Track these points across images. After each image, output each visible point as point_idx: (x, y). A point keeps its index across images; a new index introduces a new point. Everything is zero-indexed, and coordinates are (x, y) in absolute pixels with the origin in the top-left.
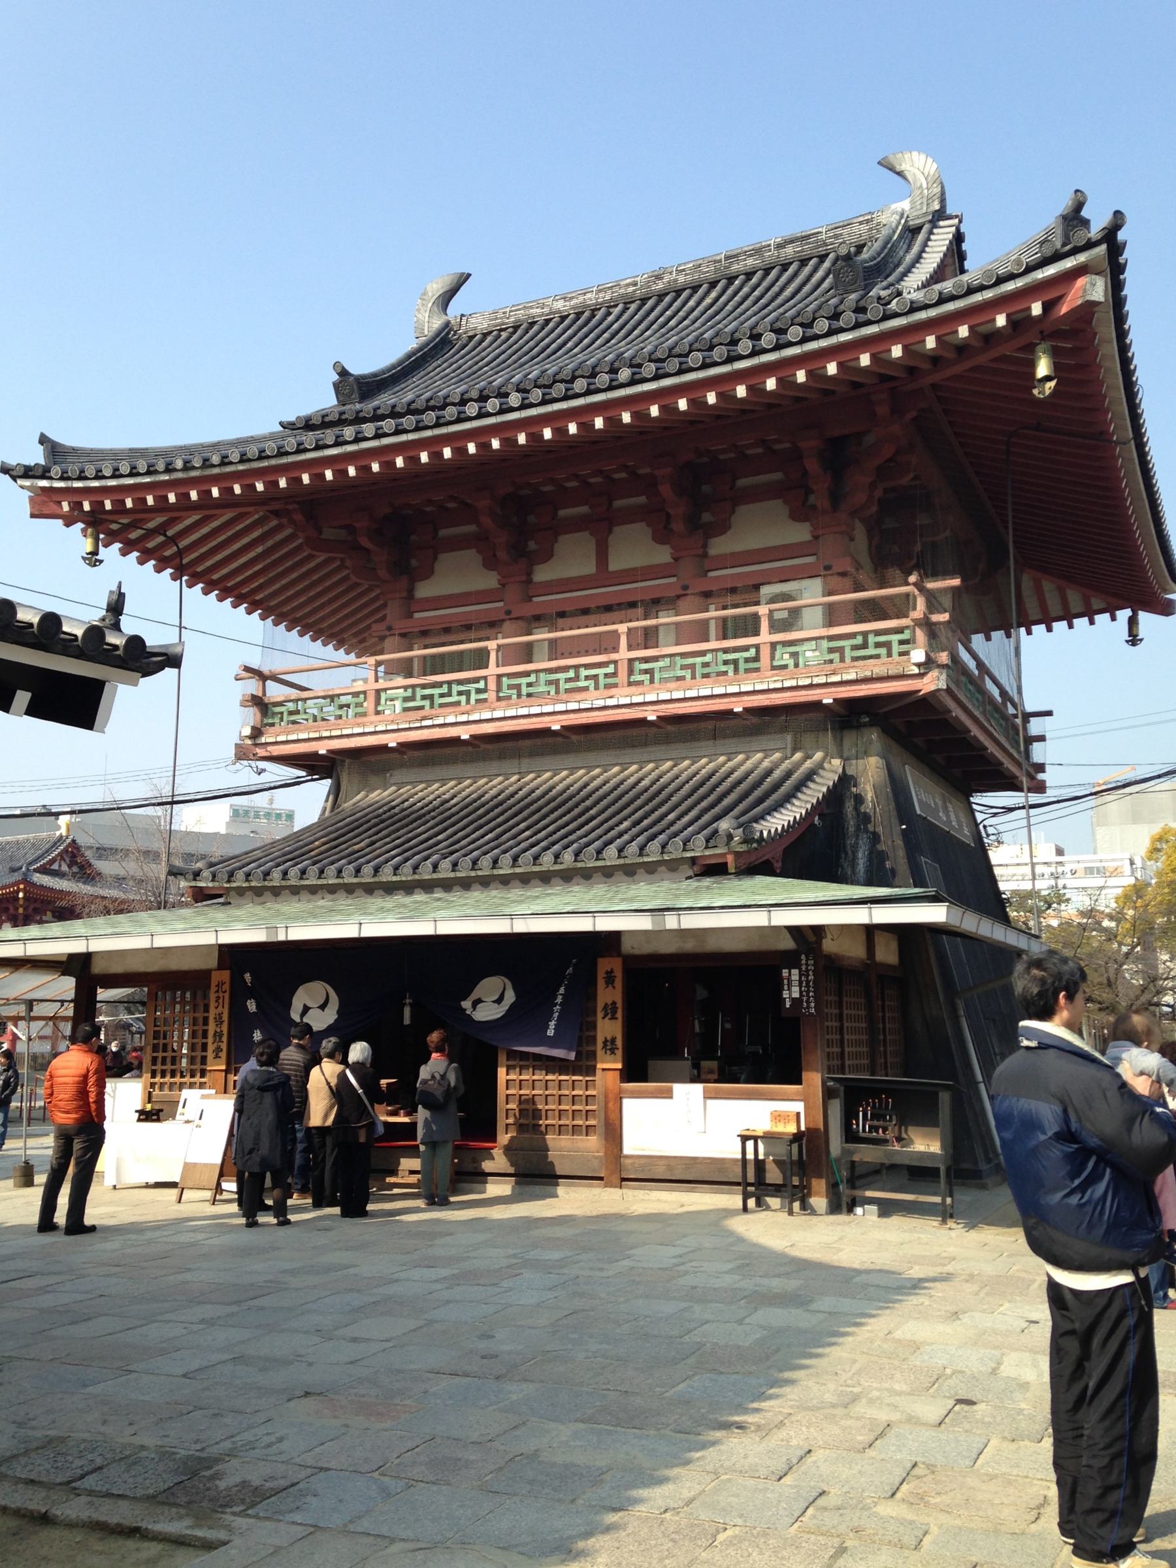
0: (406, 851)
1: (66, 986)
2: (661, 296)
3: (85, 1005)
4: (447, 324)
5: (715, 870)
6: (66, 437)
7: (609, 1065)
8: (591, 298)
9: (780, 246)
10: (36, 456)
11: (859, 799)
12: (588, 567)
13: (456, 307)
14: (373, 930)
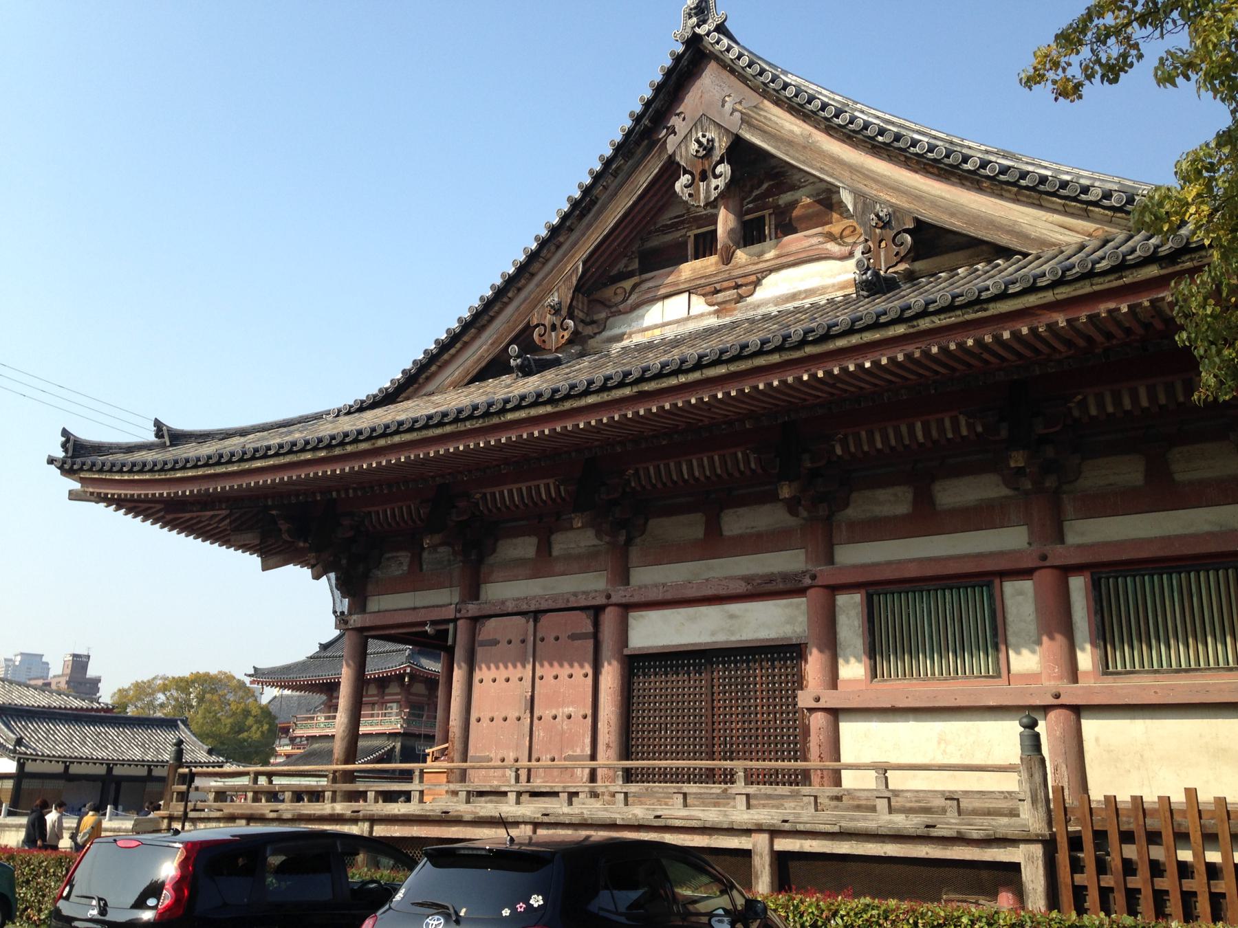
10: (252, 672)
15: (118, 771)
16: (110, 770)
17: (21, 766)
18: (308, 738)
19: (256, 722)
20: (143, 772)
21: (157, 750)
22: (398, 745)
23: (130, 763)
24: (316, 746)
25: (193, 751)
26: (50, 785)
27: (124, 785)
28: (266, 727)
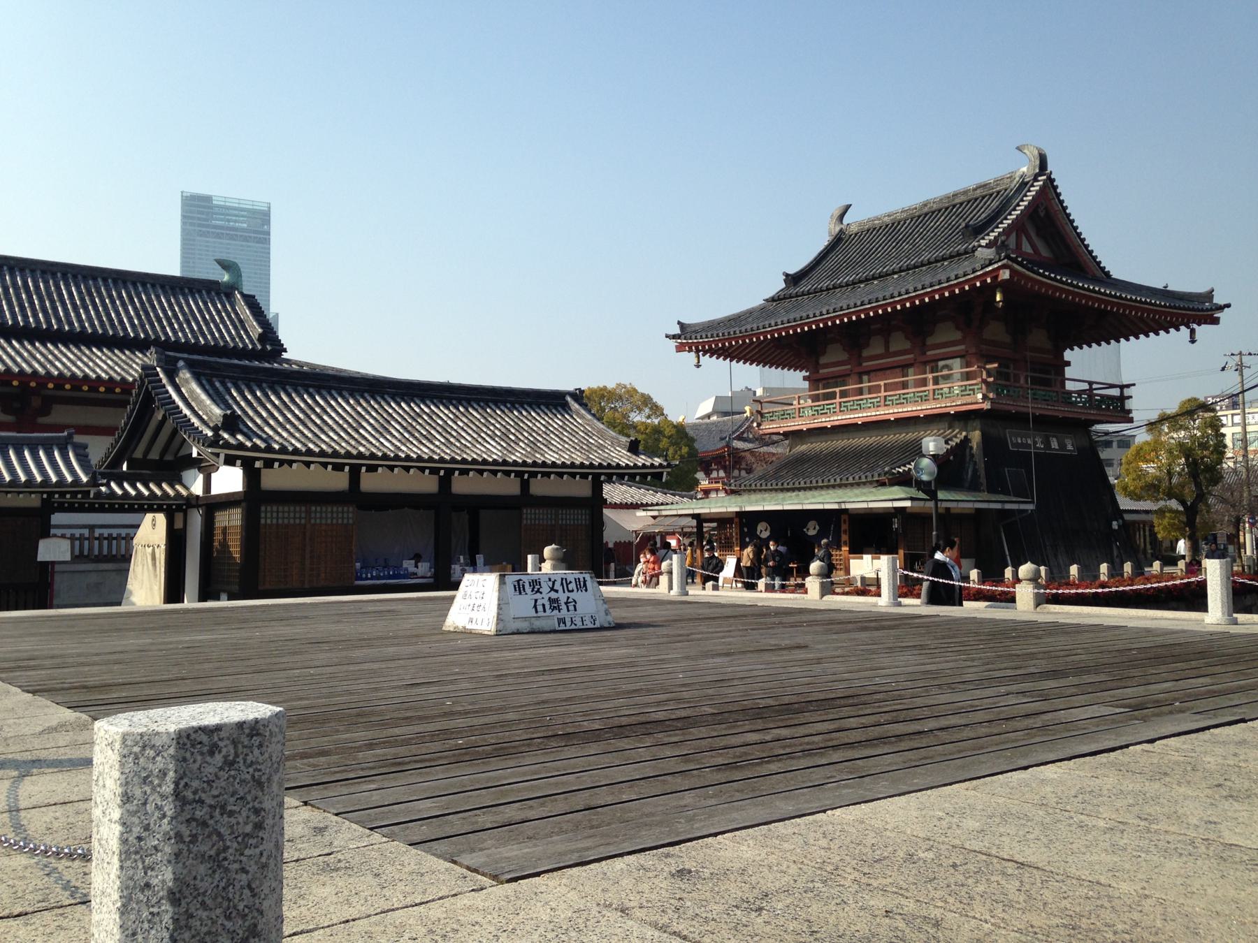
0: (796, 475)
1: (694, 523)
2: (926, 214)
3: (699, 526)
4: (841, 230)
5: (883, 484)
6: (686, 321)
7: (845, 549)
8: (899, 216)
9: (975, 190)
10: (677, 331)
11: (971, 448)
12: (880, 350)
13: (846, 221)
14: (767, 508)
15: (460, 485)
16: (445, 482)
17: (252, 476)
18: (786, 435)
19: (672, 444)
20: (511, 487)
21: (533, 445)
22: (976, 436)
23: (482, 467)
24: (803, 448)
25: (601, 447)
26: (325, 516)
27: (484, 515)
28: (685, 450)
